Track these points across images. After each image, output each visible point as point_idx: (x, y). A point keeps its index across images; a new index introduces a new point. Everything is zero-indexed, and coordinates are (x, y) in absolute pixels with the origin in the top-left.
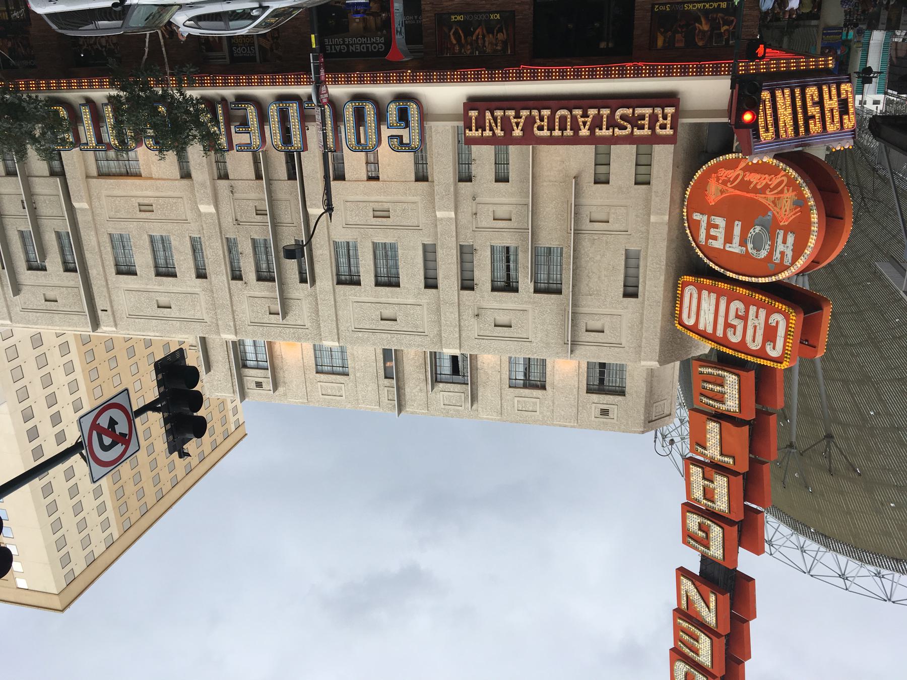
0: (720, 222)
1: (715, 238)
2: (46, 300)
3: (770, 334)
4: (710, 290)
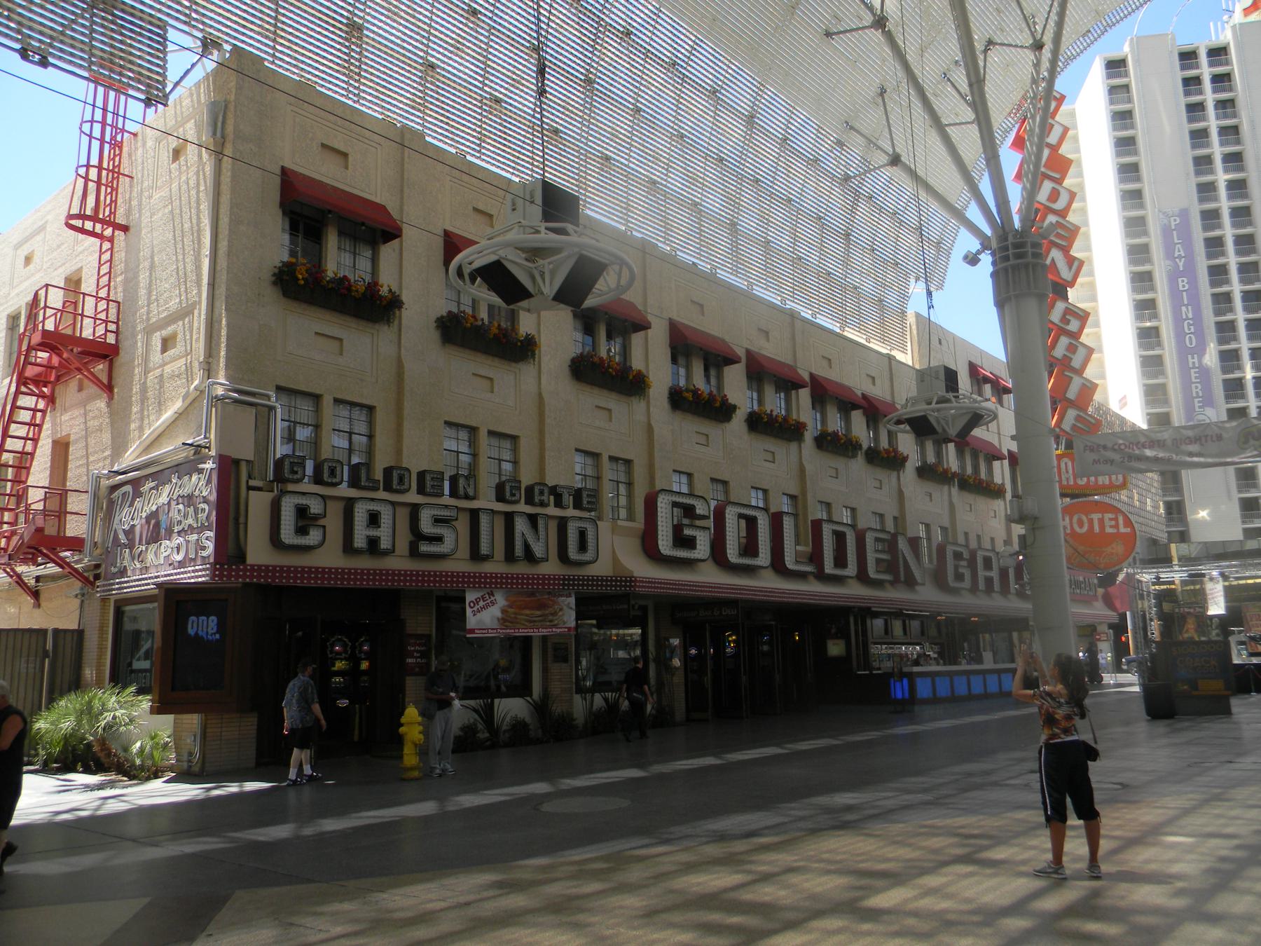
0: (1109, 530)
1: (1111, 519)
2: (345, 155)
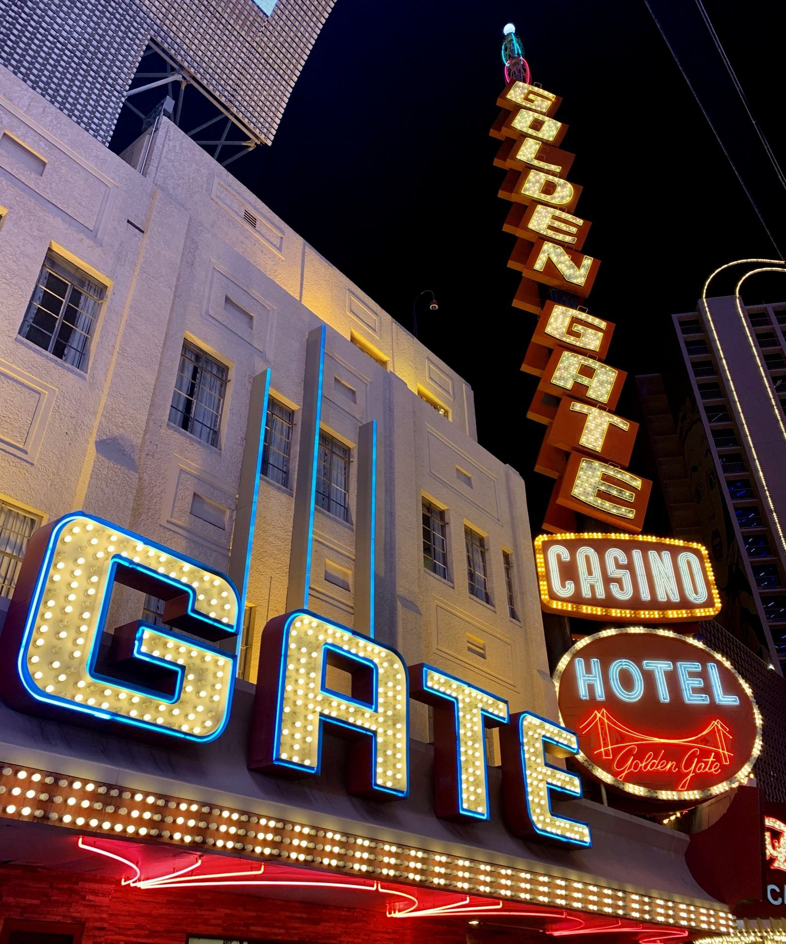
1: (692, 675)
3: (569, 572)
4: (669, 605)
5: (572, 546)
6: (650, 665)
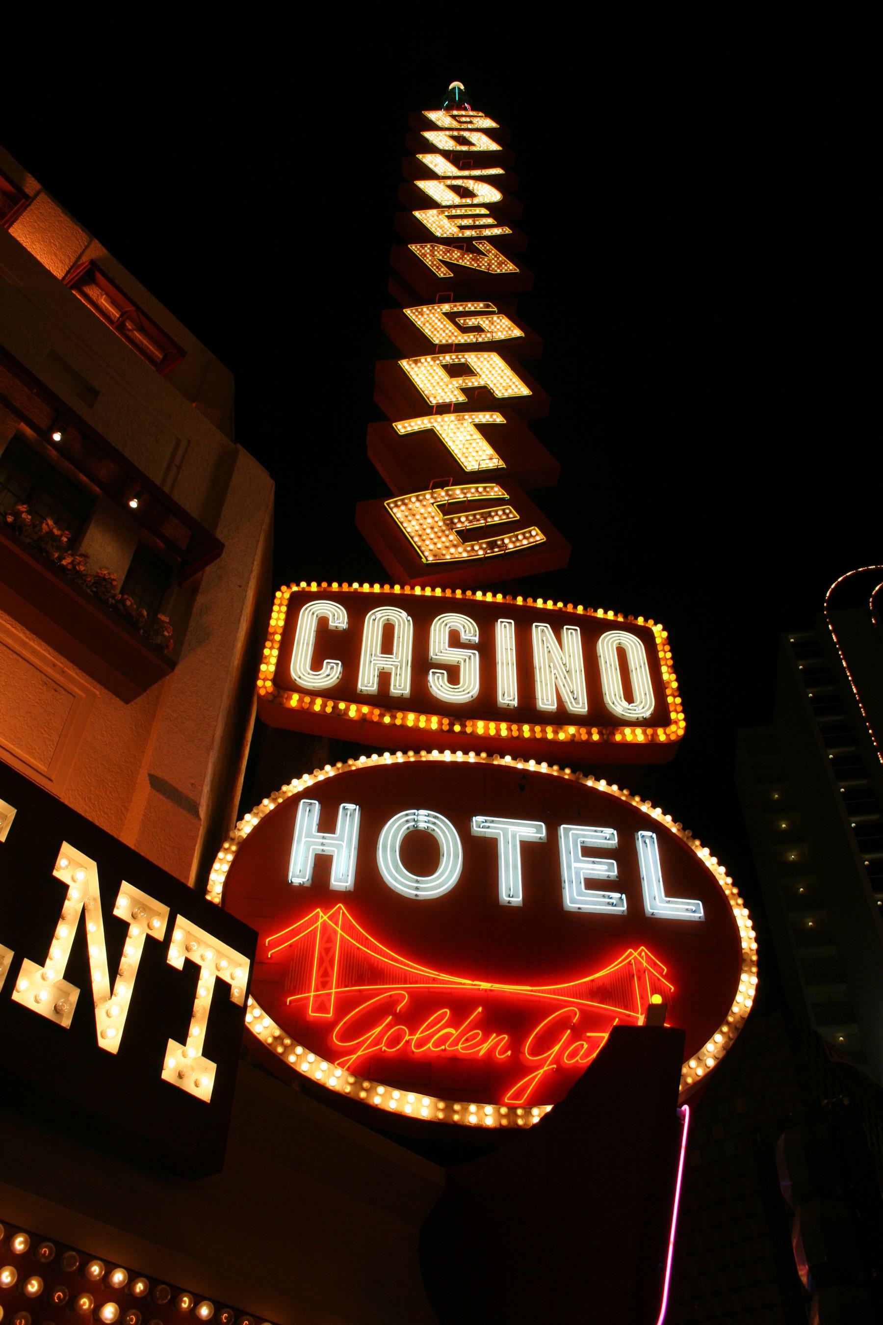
3: (338, 646)
5: (358, 607)
6: (481, 825)
